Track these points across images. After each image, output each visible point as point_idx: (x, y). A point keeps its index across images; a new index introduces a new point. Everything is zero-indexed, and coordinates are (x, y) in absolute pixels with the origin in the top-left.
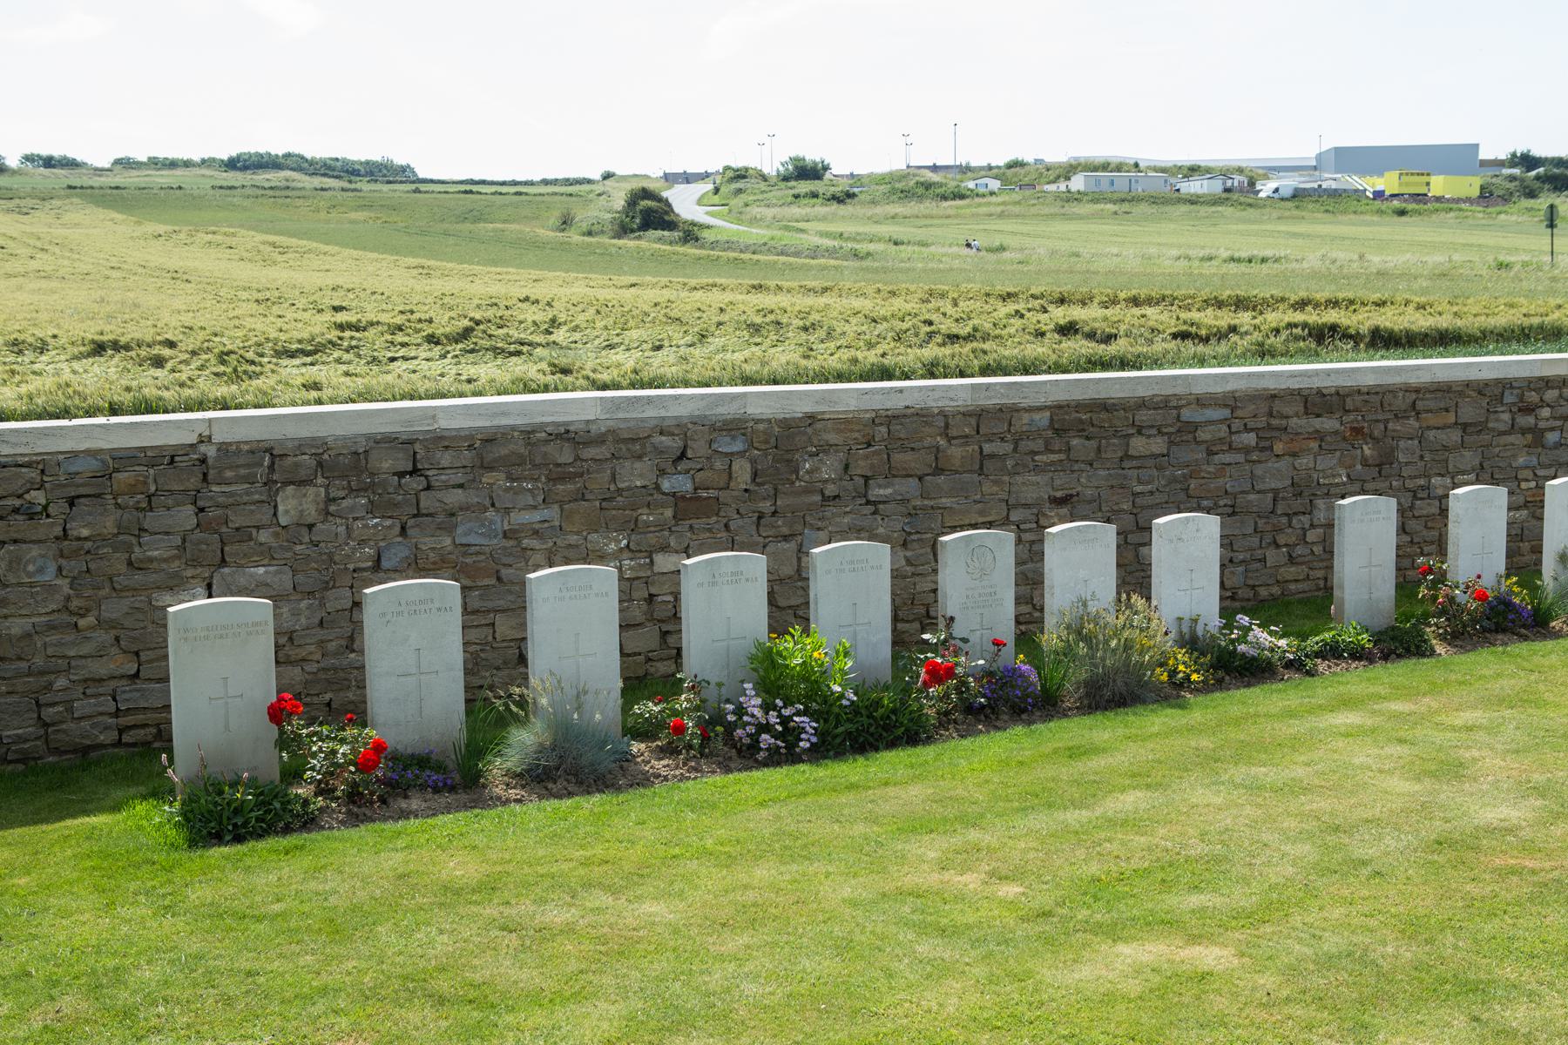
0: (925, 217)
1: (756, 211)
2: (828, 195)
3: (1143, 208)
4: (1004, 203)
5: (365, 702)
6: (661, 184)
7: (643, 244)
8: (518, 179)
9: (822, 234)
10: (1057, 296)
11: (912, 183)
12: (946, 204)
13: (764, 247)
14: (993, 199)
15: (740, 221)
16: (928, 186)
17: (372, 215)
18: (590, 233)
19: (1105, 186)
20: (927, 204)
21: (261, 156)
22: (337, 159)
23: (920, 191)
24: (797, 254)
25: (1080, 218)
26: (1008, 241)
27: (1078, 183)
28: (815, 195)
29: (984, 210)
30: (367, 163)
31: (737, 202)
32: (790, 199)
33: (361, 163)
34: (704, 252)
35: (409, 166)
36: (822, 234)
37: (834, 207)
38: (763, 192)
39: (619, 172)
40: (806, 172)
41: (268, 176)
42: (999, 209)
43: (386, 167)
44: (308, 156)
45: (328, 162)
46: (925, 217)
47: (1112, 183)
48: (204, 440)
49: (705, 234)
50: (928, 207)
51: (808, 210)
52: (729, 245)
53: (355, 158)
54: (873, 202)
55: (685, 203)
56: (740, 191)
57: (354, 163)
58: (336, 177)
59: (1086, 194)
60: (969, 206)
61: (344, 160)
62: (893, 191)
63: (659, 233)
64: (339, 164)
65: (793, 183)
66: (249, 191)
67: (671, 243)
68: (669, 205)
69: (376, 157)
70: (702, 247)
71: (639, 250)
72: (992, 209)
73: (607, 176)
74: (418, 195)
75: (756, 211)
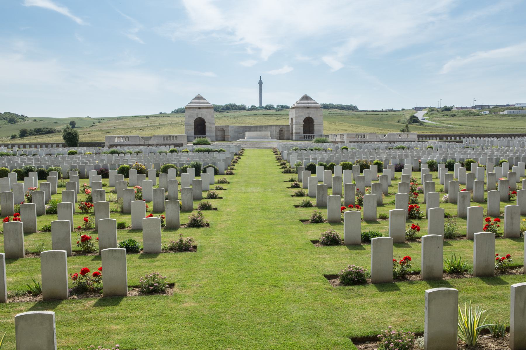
0: (470, 120)
1: (435, 118)
2: (450, 115)
3: (520, 118)
4: (488, 117)
6: (414, 111)
7: (413, 125)
8: (377, 110)
9: (447, 124)
11: (468, 113)
12: (475, 117)
13: (435, 126)
14: (486, 116)
15: (431, 121)
16: (472, 113)
18: (403, 123)
19: (512, 113)
20: (471, 117)
21: (325, 104)
22: (340, 105)
23: (470, 114)
24: (440, 128)
25: (503, 120)
26: (480, 125)
27: (506, 112)
28: (447, 115)
29: (483, 118)
30: (347, 105)
31: (431, 116)
32: (442, 116)
34: (424, 127)
36: (447, 124)
37: (451, 118)
38: (437, 114)
39: (406, 109)
40: (447, 109)
41: (332, 110)
42: (486, 118)
43: (351, 106)
46: (470, 120)
47: (514, 112)
48: (214, 194)
49: (424, 124)
50: (471, 118)
51: (446, 118)
52: (428, 126)
53: (344, 104)
54: (460, 117)
55: (420, 115)
56: (432, 114)
57: (344, 105)
59: (507, 115)
60: (480, 117)
61: (342, 105)
62: (464, 114)
63: (416, 124)
65: (444, 112)
66: (335, 114)
67: (418, 125)
68: (418, 119)
70: (424, 126)
71: (413, 127)
72: (485, 118)
73: (403, 110)
75: (435, 118)
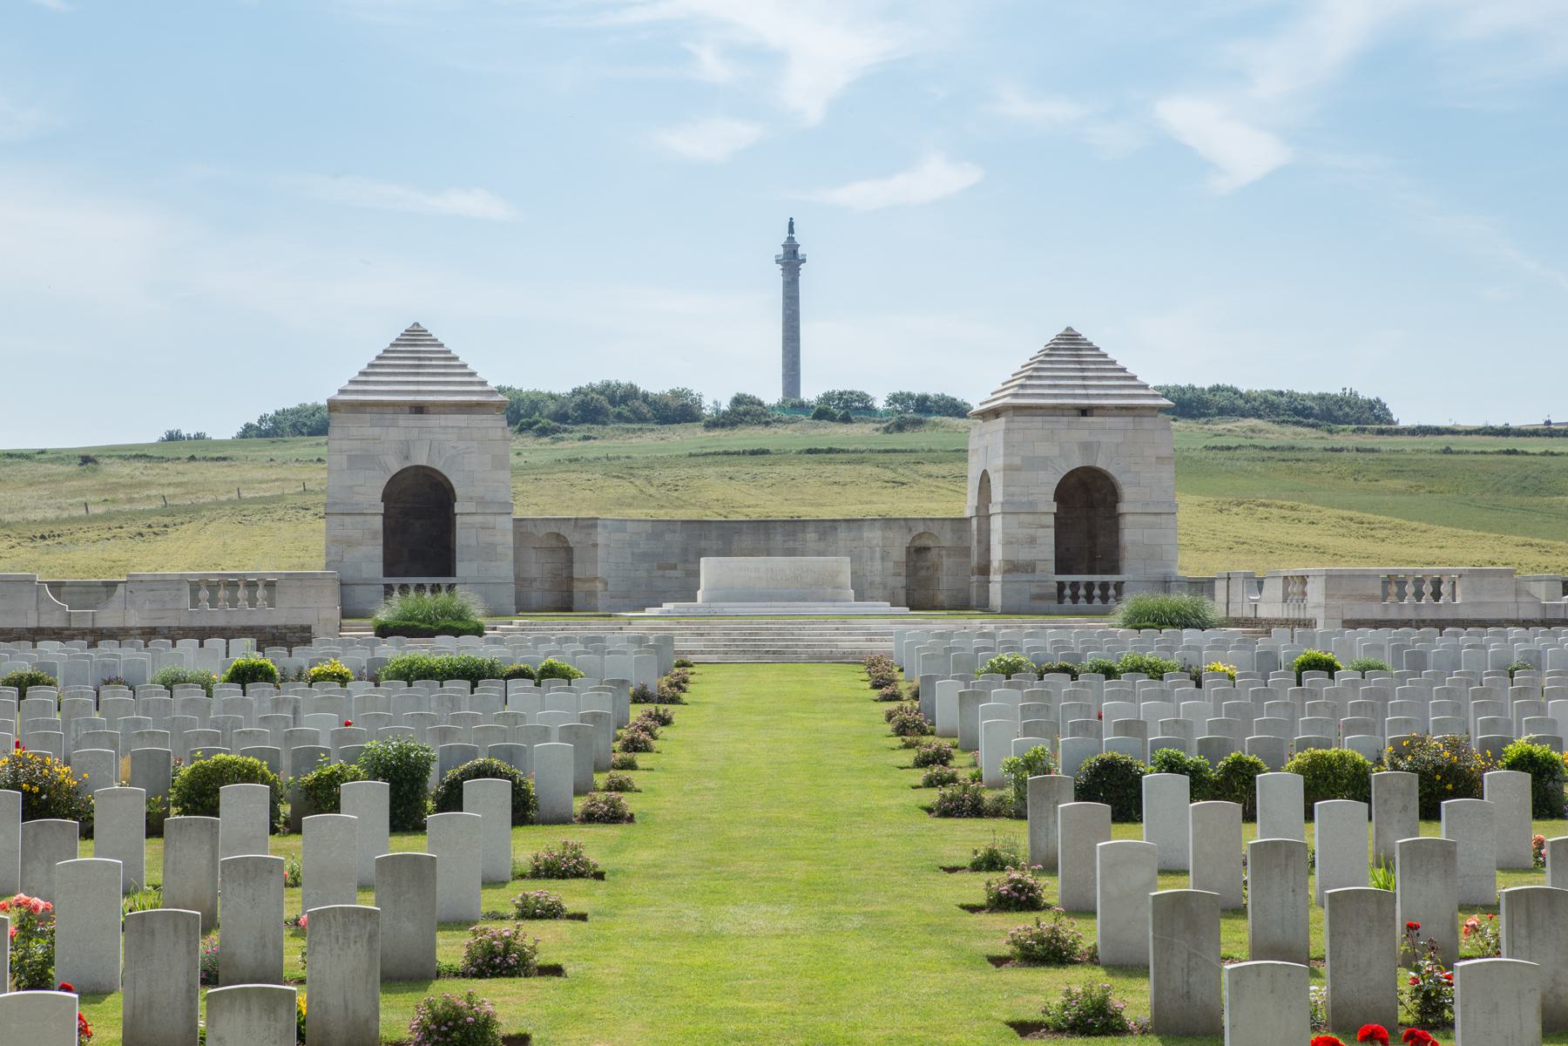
5: (526, 976)
8: (1515, 423)
10: (688, 454)
17: (1413, 484)
22: (1281, 393)
33: (1314, 398)
35: (1378, 401)
41: (1229, 426)
43: (1348, 403)
44: (1243, 389)
45: (1271, 397)
58: (1313, 426)
61: (1291, 395)
64: (1284, 400)
69: (1335, 390)
74: (1450, 457)
